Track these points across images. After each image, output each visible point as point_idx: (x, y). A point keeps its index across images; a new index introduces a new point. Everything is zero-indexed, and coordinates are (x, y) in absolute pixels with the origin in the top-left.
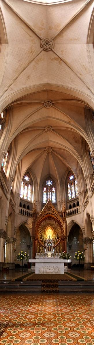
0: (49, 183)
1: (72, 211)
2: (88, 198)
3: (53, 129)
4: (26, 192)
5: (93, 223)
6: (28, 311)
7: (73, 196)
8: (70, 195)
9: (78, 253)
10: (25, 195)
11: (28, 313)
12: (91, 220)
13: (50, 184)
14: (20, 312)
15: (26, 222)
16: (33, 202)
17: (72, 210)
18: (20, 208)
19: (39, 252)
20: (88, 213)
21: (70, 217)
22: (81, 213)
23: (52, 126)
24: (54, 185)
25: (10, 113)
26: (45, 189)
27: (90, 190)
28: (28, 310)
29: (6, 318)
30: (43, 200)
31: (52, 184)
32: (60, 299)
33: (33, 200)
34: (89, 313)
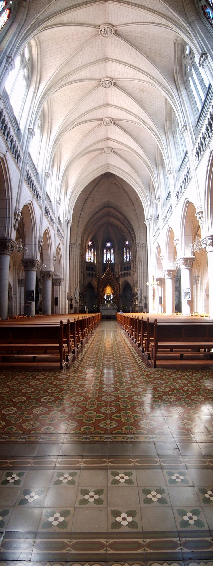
0: (109, 245)
3: (114, 123)
4: (90, 255)
6: (78, 377)
7: (128, 259)
8: (125, 258)
9: (123, 306)
10: (89, 258)
11: (72, 394)
13: (110, 245)
14: (59, 392)
15: (91, 281)
16: (95, 264)
17: (125, 272)
18: (87, 272)
19: (102, 303)
20: (170, 228)
21: (124, 277)
22: (131, 276)
24: (112, 247)
25: (153, 451)
26: (105, 250)
27: (192, 153)
28: (72, 389)
29: (27, 413)
30: (103, 260)
32: (125, 366)
33: (95, 262)
34: (186, 393)
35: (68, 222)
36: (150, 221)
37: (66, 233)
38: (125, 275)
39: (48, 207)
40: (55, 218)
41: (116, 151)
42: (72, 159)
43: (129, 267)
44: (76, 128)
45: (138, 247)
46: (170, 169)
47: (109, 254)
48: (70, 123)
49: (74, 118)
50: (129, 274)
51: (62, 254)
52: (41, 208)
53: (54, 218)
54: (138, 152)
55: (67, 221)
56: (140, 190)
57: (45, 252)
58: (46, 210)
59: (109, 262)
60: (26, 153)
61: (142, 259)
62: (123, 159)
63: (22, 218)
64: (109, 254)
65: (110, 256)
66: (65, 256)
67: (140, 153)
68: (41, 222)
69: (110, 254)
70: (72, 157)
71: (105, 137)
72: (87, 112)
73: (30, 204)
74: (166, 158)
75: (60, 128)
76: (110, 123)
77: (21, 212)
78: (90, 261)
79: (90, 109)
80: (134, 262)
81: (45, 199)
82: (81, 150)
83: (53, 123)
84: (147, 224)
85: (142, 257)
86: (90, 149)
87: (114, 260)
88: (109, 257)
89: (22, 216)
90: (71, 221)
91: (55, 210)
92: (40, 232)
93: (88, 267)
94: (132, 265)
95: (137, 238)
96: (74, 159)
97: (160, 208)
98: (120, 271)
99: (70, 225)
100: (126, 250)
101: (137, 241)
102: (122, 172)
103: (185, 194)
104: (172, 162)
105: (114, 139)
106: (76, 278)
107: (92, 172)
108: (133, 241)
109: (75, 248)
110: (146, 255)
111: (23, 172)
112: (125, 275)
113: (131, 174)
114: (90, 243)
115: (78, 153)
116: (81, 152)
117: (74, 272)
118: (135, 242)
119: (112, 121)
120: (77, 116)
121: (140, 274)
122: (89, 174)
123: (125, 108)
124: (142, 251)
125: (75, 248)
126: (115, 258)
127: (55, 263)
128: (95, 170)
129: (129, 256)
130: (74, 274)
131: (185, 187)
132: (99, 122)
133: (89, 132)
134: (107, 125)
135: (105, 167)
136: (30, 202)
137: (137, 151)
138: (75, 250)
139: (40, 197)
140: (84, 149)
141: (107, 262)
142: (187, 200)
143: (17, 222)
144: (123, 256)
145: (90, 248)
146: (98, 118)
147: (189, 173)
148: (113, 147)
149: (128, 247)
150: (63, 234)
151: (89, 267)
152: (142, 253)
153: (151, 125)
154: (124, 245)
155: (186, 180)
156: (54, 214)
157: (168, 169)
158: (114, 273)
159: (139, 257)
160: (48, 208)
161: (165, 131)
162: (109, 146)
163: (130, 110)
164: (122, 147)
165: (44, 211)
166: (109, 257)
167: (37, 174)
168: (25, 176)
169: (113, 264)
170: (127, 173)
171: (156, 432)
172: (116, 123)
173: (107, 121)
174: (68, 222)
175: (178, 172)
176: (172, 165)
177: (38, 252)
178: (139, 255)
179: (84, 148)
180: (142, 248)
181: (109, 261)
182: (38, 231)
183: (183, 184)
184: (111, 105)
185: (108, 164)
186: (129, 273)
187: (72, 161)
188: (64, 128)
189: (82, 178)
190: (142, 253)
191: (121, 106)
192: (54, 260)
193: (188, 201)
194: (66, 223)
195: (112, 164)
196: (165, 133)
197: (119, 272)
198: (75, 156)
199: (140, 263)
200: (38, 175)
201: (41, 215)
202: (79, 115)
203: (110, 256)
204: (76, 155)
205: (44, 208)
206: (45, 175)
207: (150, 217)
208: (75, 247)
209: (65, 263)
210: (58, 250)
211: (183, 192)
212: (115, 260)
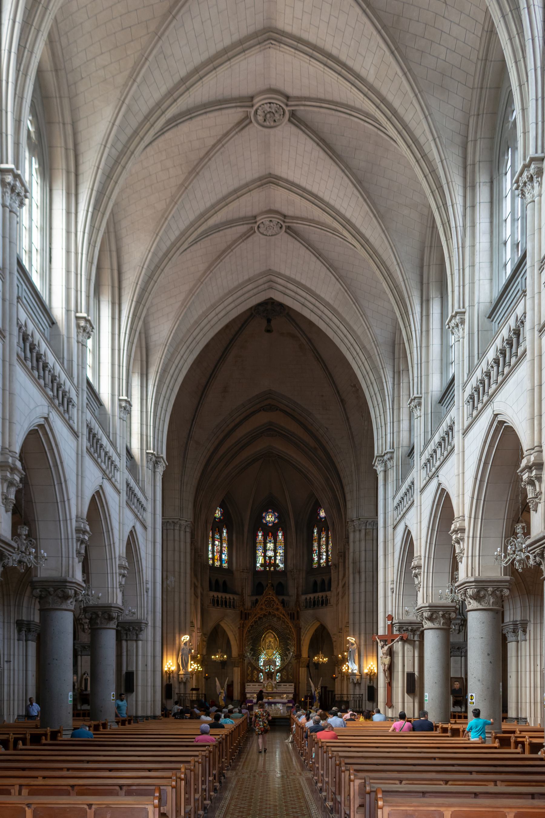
0: (270, 518)
1: (316, 598)
2: (517, 333)
3: (293, 114)
5: (538, 495)
10: (217, 556)
12: (525, 477)
13: (268, 519)
18: (212, 594)
20: (443, 490)
23: (289, 91)
30: (255, 562)
31: (276, 521)
35: (156, 463)
36: (388, 462)
37: (149, 494)
38: (314, 605)
39: (97, 426)
40: (119, 455)
41: (299, 226)
42: (156, 260)
43: (326, 582)
44: (162, 138)
45: (351, 529)
46: (462, 310)
47: (270, 546)
48: (141, 124)
49: (151, 103)
50: (324, 603)
51: (143, 554)
52: (76, 434)
53: (115, 457)
54: (368, 233)
55: (154, 459)
56: (366, 364)
57: (93, 554)
58: (92, 436)
59: (272, 569)
60: (8, 266)
61: (363, 564)
62: (319, 254)
63: (26, 476)
64: (270, 546)
65: (275, 551)
66: (150, 559)
67: (372, 240)
68: (80, 475)
69: (275, 543)
70: (155, 254)
71: (259, 27)
72: (196, 70)
73: (41, 426)
74: (456, 283)
75: (109, 145)
76: (277, 116)
77: (21, 460)
78: (217, 564)
79: (205, 56)
80: (341, 569)
81: (85, 405)
82: (182, 227)
83: (82, 125)
84: (379, 468)
85: (363, 559)
86: (211, 222)
87: (285, 562)
88: (270, 553)
89: (24, 468)
90: (165, 457)
91: (118, 432)
92: (80, 495)
93: (213, 582)
94: (334, 575)
95: (349, 505)
96: (161, 261)
97: (419, 425)
98: (300, 593)
99: (160, 470)
100: (319, 534)
101: (349, 512)
102: (313, 300)
103: (498, 398)
104: (472, 283)
105: (291, 178)
106: (182, 575)
107: (222, 300)
108: (339, 510)
109: (177, 532)
110: (375, 563)
111: (10, 334)
112: (314, 605)
113: (340, 310)
114: (218, 514)
115: (173, 238)
116: (183, 234)
117: (177, 599)
118: (345, 514)
119: (287, 109)
120: (164, 90)
121: (357, 605)
122: (213, 307)
123: (335, 52)
124: (363, 543)
125: (177, 532)
126: (289, 556)
127: (123, 583)
128: (231, 292)
129: (327, 552)
130: (177, 603)
131: (500, 379)
132: (239, 110)
133: (207, 153)
134: (267, 124)
135: (261, 281)
136: (42, 421)
137: (363, 230)
138: (177, 538)
139: (70, 401)
140: (192, 224)
141: (265, 568)
142: (500, 418)
143: (13, 490)
144: (311, 552)
145: (217, 527)
146: (236, 93)
147: (518, 338)
148: (286, 212)
149: (323, 526)
150: (142, 499)
151: (217, 582)
152: (363, 548)
153: (418, 133)
154: (314, 520)
155: (505, 357)
156: (113, 444)
157: (456, 309)
158: (286, 598)
159: (354, 559)
160: (97, 429)
161: (465, 158)
162: (273, 207)
163: (350, 63)
164: (317, 213)
165: (85, 442)
166: (270, 553)
167: (53, 323)
168: (18, 343)
169: (283, 573)
170: (327, 305)
171: (376, 671)
172: (298, 114)
173: (267, 107)
174: (156, 463)
175: (486, 319)
176: (472, 292)
177: (76, 560)
178: (354, 553)
179: (192, 217)
180: (363, 532)
181: (270, 565)
182: (73, 502)
183: (495, 368)
184: (283, 33)
185: (269, 272)
186: (327, 600)
187: (157, 267)
188: (120, 146)
189: (192, 321)
190: (363, 548)
191: (320, 44)
192: (120, 574)
193: (505, 422)
194: (151, 466)
195: (282, 272)
196: (465, 168)
197: (298, 595)
198: (164, 249)
199: (357, 576)
200: (58, 328)
201: (77, 454)
202: (170, 84)
203: (275, 551)
204: (168, 243)
205: (85, 431)
206: (78, 326)
207: (388, 450)
208: (177, 527)
209: (150, 578)
210: (132, 537)
211: (491, 391)
212: (289, 562)
